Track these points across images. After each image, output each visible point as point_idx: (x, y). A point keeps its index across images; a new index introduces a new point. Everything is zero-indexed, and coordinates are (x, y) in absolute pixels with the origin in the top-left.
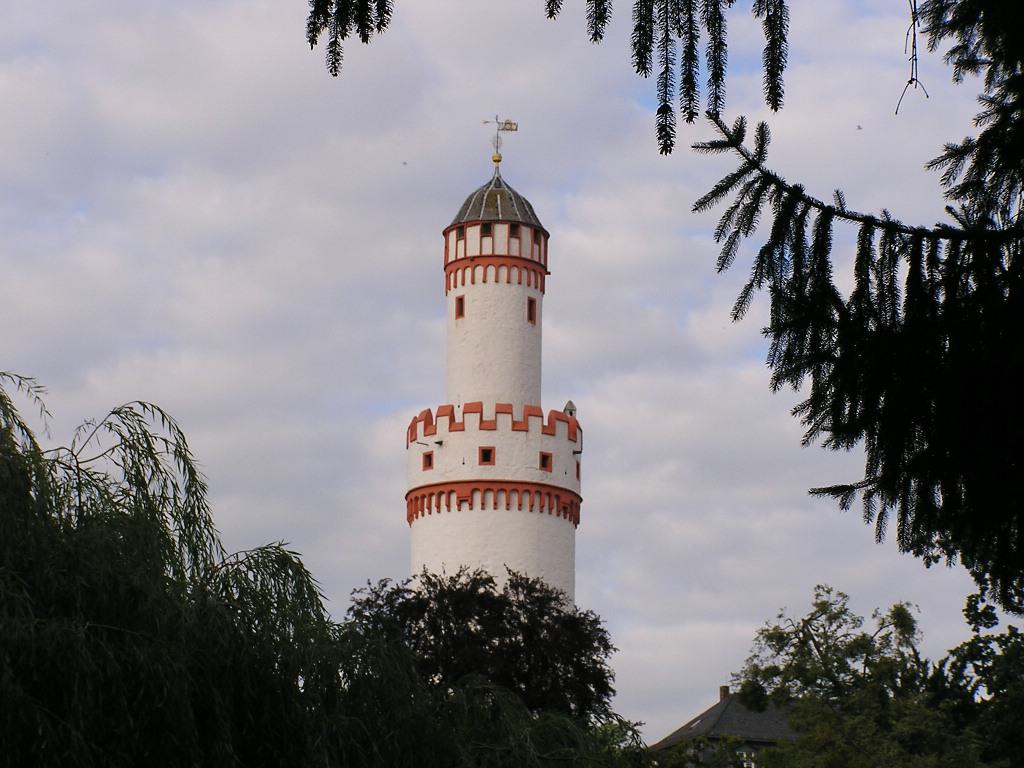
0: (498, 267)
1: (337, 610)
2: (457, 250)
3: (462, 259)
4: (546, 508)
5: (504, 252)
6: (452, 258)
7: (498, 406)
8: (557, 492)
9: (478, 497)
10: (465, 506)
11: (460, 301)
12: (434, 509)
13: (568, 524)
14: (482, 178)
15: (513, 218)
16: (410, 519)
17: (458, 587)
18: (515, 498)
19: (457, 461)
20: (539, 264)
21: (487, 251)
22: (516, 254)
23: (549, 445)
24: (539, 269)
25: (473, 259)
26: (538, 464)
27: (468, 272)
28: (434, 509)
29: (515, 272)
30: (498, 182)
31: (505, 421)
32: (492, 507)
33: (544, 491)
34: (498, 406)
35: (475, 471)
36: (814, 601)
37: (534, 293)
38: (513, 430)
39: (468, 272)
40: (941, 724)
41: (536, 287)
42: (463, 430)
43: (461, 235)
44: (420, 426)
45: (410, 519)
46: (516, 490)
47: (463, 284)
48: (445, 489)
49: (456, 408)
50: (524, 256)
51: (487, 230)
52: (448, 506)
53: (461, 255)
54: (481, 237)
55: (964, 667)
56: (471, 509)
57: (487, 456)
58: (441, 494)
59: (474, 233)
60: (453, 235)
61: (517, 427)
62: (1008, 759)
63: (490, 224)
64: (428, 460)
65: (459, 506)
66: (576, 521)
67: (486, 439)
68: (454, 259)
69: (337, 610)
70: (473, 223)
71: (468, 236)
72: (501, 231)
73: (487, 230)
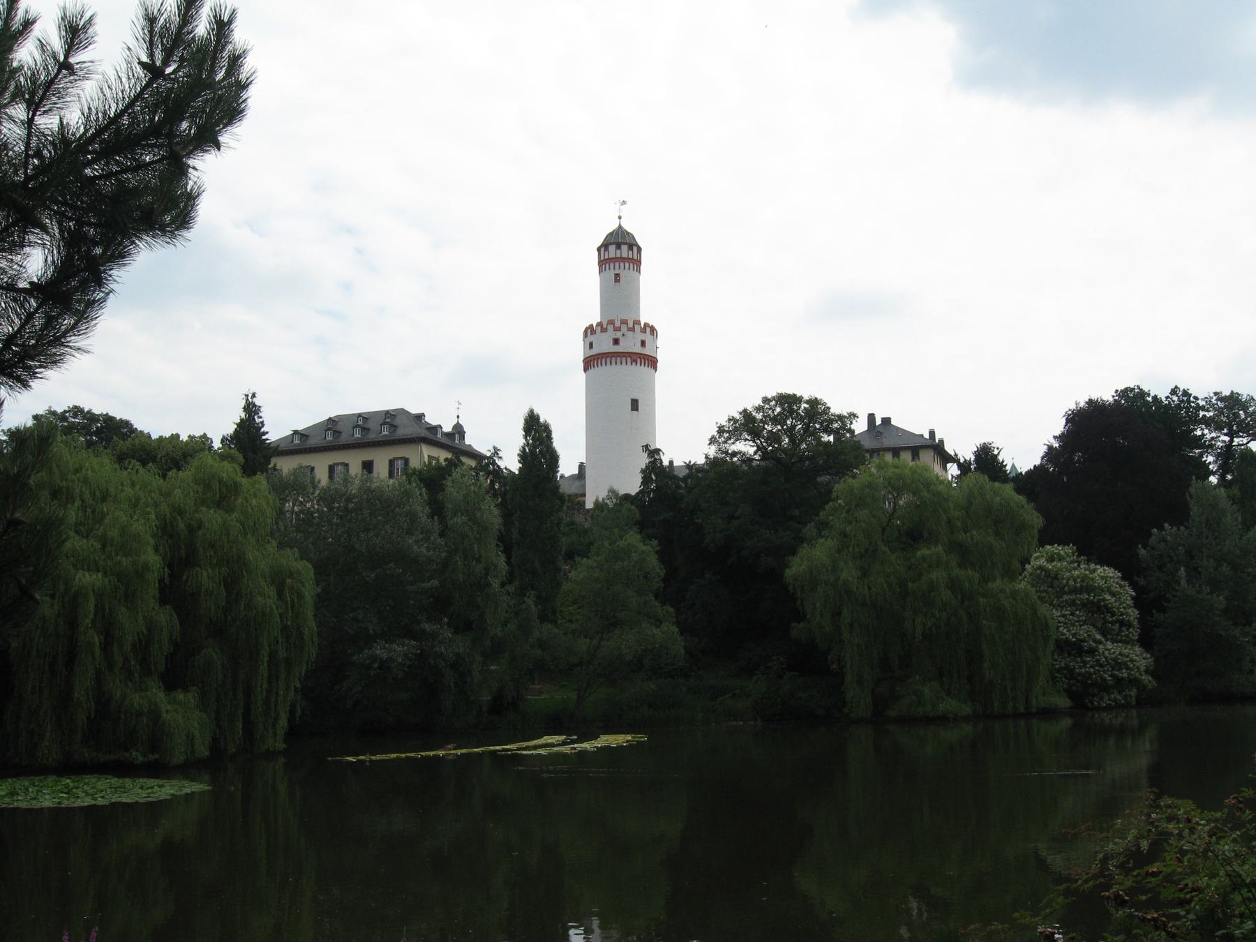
3: (612, 258)
4: (643, 365)
6: (602, 258)
10: (634, 364)
11: (617, 275)
12: (596, 366)
13: (654, 371)
14: (613, 226)
16: (251, 409)
18: (619, 360)
19: (604, 344)
20: (637, 260)
21: (618, 255)
22: (619, 256)
23: (642, 336)
25: (624, 258)
27: (607, 266)
28: (596, 366)
30: (620, 226)
31: (624, 328)
35: (637, 349)
36: (750, 409)
39: (607, 266)
40: (92, 549)
44: (589, 331)
45: (251, 409)
46: (614, 356)
47: (609, 269)
49: (616, 321)
50: (623, 256)
53: (606, 257)
57: (616, 342)
58: (598, 358)
59: (612, 248)
60: (603, 249)
64: (591, 345)
67: (642, 336)
72: (625, 248)
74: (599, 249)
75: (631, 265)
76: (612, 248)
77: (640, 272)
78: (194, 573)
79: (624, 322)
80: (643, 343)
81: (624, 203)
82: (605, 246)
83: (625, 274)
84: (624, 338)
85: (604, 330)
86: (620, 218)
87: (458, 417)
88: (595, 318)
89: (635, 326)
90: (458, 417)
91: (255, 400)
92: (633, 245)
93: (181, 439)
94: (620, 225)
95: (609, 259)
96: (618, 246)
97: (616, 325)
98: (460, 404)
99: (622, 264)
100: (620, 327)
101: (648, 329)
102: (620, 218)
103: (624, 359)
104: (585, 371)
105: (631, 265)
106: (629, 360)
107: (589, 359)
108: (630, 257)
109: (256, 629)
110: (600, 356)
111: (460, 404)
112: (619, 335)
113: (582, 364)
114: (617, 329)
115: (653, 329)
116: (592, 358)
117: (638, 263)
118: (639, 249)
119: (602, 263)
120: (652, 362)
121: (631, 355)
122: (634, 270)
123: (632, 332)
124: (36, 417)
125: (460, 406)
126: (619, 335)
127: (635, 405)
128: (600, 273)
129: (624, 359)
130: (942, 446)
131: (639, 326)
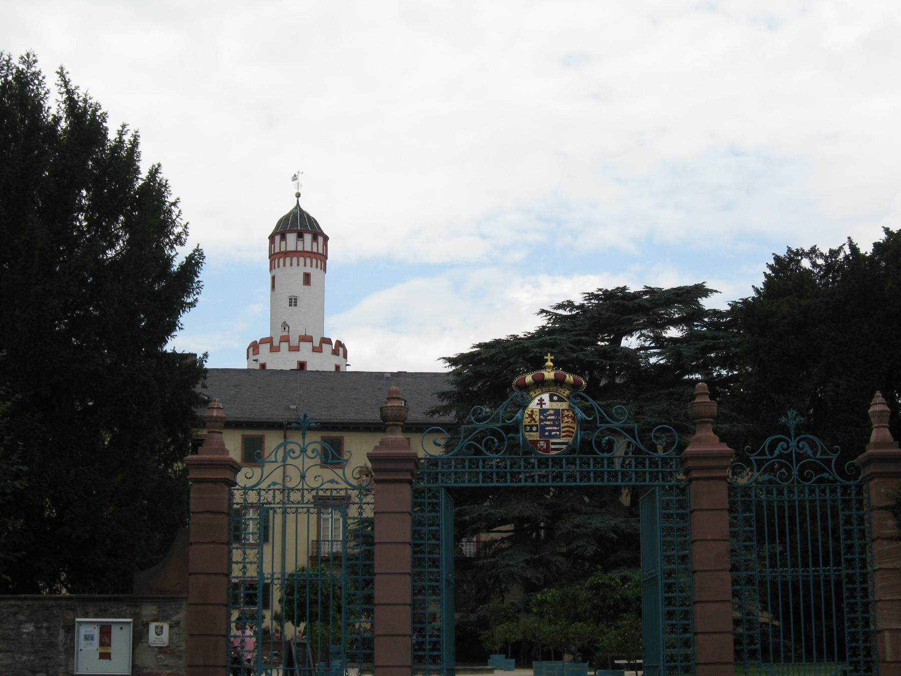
1: (176, 344)
2: (280, 246)
5: (293, 249)
6: (277, 250)
14: (286, 208)
20: (322, 255)
21: (300, 248)
24: (322, 258)
27: (282, 261)
38: (289, 351)
39: (282, 261)
41: (321, 269)
42: (279, 351)
43: (283, 238)
44: (251, 350)
47: (284, 266)
50: (289, 249)
51: (300, 236)
53: (283, 249)
54: (297, 240)
55: (189, 303)
59: (291, 238)
60: (278, 238)
62: (82, 191)
63: (284, 233)
68: (279, 251)
69: (176, 344)
70: (291, 231)
72: (308, 237)
73: (300, 236)
74: (272, 238)
76: (291, 238)
77: (325, 270)
78: (811, 569)
81: (295, 178)
83: (315, 273)
89: (324, 345)
91: (302, 270)
92: (317, 233)
93: (895, 232)
99: (308, 260)
100: (299, 347)
102: (298, 195)
108: (315, 250)
118: (326, 239)
119: (275, 257)
122: (317, 267)
124: (186, 258)
129: (302, 260)
131: (329, 346)
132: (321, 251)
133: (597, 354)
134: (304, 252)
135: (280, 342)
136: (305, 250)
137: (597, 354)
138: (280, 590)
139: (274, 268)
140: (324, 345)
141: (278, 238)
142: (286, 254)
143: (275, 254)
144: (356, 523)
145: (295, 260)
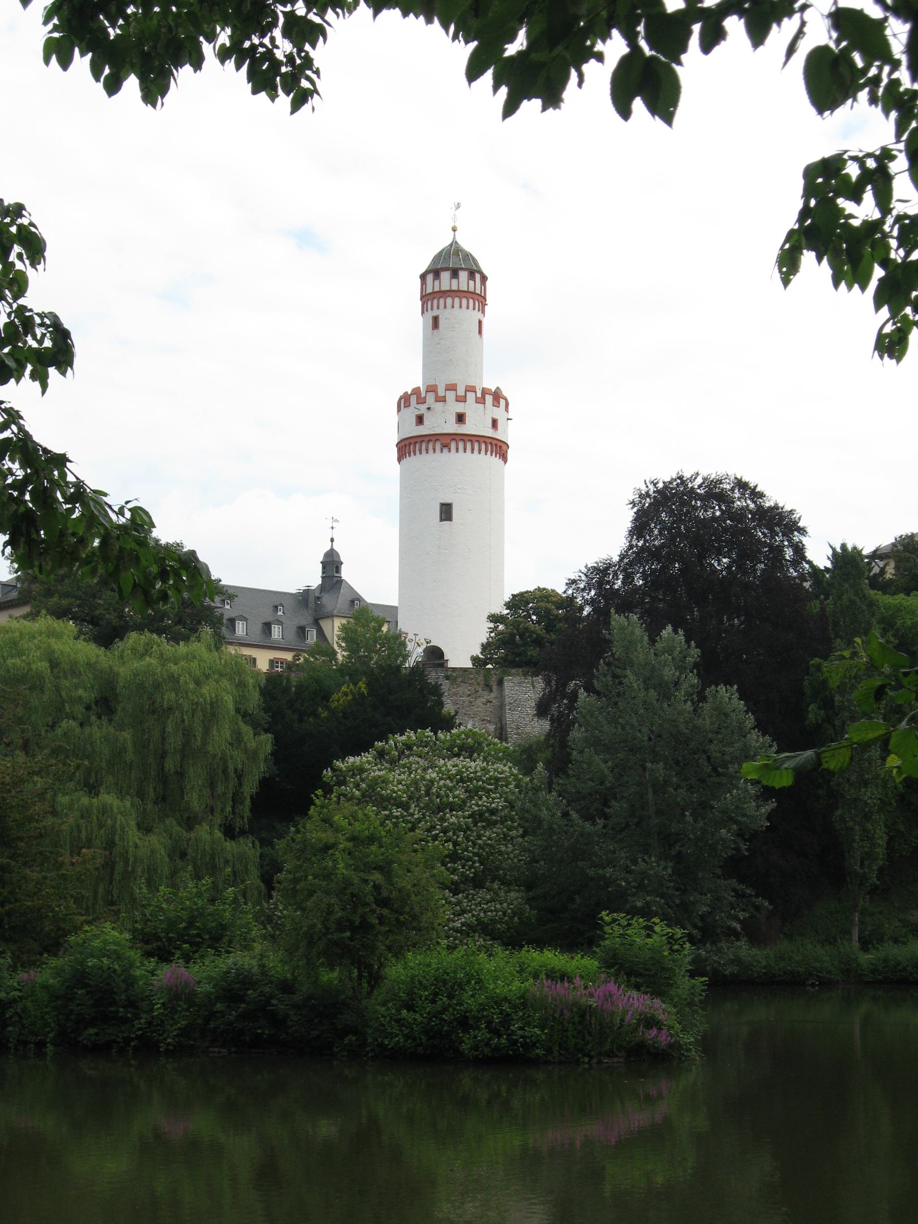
0: (460, 298)
3: (437, 292)
5: (448, 288)
6: (429, 290)
7: (466, 386)
8: (490, 440)
9: (453, 445)
13: (501, 462)
15: (470, 267)
17: (717, 490)
18: (461, 445)
21: (454, 288)
26: (490, 426)
29: (457, 300)
30: (454, 243)
32: (470, 451)
33: (488, 441)
34: (466, 386)
35: (451, 427)
37: (479, 315)
39: (435, 302)
48: (419, 440)
50: (443, 288)
52: (434, 450)
53: (437, 289)
56: (450, 452)
57: (461, 418)
58: (416, 443)
59: (445, 276)
60: (430, 278)
61: (478, 401)
64: (420, 420)
65: (442, 449)
66: (505, 459)
67: (460, 408)
68: (431, 291)
71: (442, 277)
72: (463, 275)
74: (423, 277)
75: (471, 301)
76: (445, 276)
79: (452, 387)
80: (495, 423)
82: (434, 271)
84: (430, 412)
85: (442, 399)
86: (454, 230)
87: (332, 540)
88: (414, 380)
89: (468, 393)
90: (332, 540)
92: (474, 272)
94: (454, 238)
95: (440, 292)
96: (455, 274)
97: (453, 393)
98: (336, 521)
99: (464, 301)
101: (489, 399)
102: (454, 230)
103: (461, 445)
104: (399, 460)
105: (471, 301)
106: (438, 445)
107: (407, 442)
108: (471, 289)
109: (572, 826)
110: (419, 440)
111: (336, 521)
112: (422, 409)
113: (396, 449)
114: (462, 399)
115: (497, 396)
116: (413, 441)
117: (480, 300)
118: (484, 279)
119: (427, 298)
120: (499, 449)
121: (439, 437)
123: (441, 404)
125: (335, 525)
126: (422, 409)
127: (446, 512)
128: (423, 313)
130: (336, 559)
132: (478, 291)
133: (700, 924)
134: (458, 291)
135: (426, 392)
136: (461, 289)
137: (700, 924)
138: (595, 567)
139: (427, 311)
140: (468, 393)
141: (430, 278)
142: (443, 294)
143: (426, 295)
144: (91, 835)
145: (449, 300)
